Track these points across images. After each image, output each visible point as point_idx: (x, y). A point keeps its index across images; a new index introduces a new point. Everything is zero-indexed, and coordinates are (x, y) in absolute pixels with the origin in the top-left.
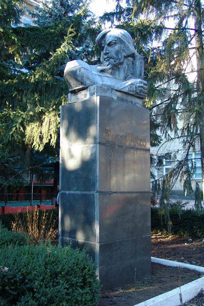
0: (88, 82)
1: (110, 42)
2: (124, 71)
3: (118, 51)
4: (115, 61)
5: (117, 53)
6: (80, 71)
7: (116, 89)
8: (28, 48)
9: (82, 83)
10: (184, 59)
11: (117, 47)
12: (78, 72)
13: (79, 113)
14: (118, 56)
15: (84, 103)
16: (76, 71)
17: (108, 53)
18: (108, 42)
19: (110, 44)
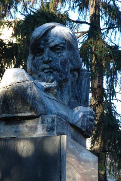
0: (40, 108)
1: (57, 45)
2: (69, 92)
3: (66, 61)
4: (61, 76)
5: (64, 63)
6: (31, 88)
7: (71, 122)
8: (11, 47)
9: (32, 109)
10: (11, 64)
11: (65, 54)
12: (29, 91)
13: (27, 159)
14: (65, 69)
15: (38, 143)
16: (27, 87)
17: (51, 61)
18: (52, 44)
19: (54, 48)
